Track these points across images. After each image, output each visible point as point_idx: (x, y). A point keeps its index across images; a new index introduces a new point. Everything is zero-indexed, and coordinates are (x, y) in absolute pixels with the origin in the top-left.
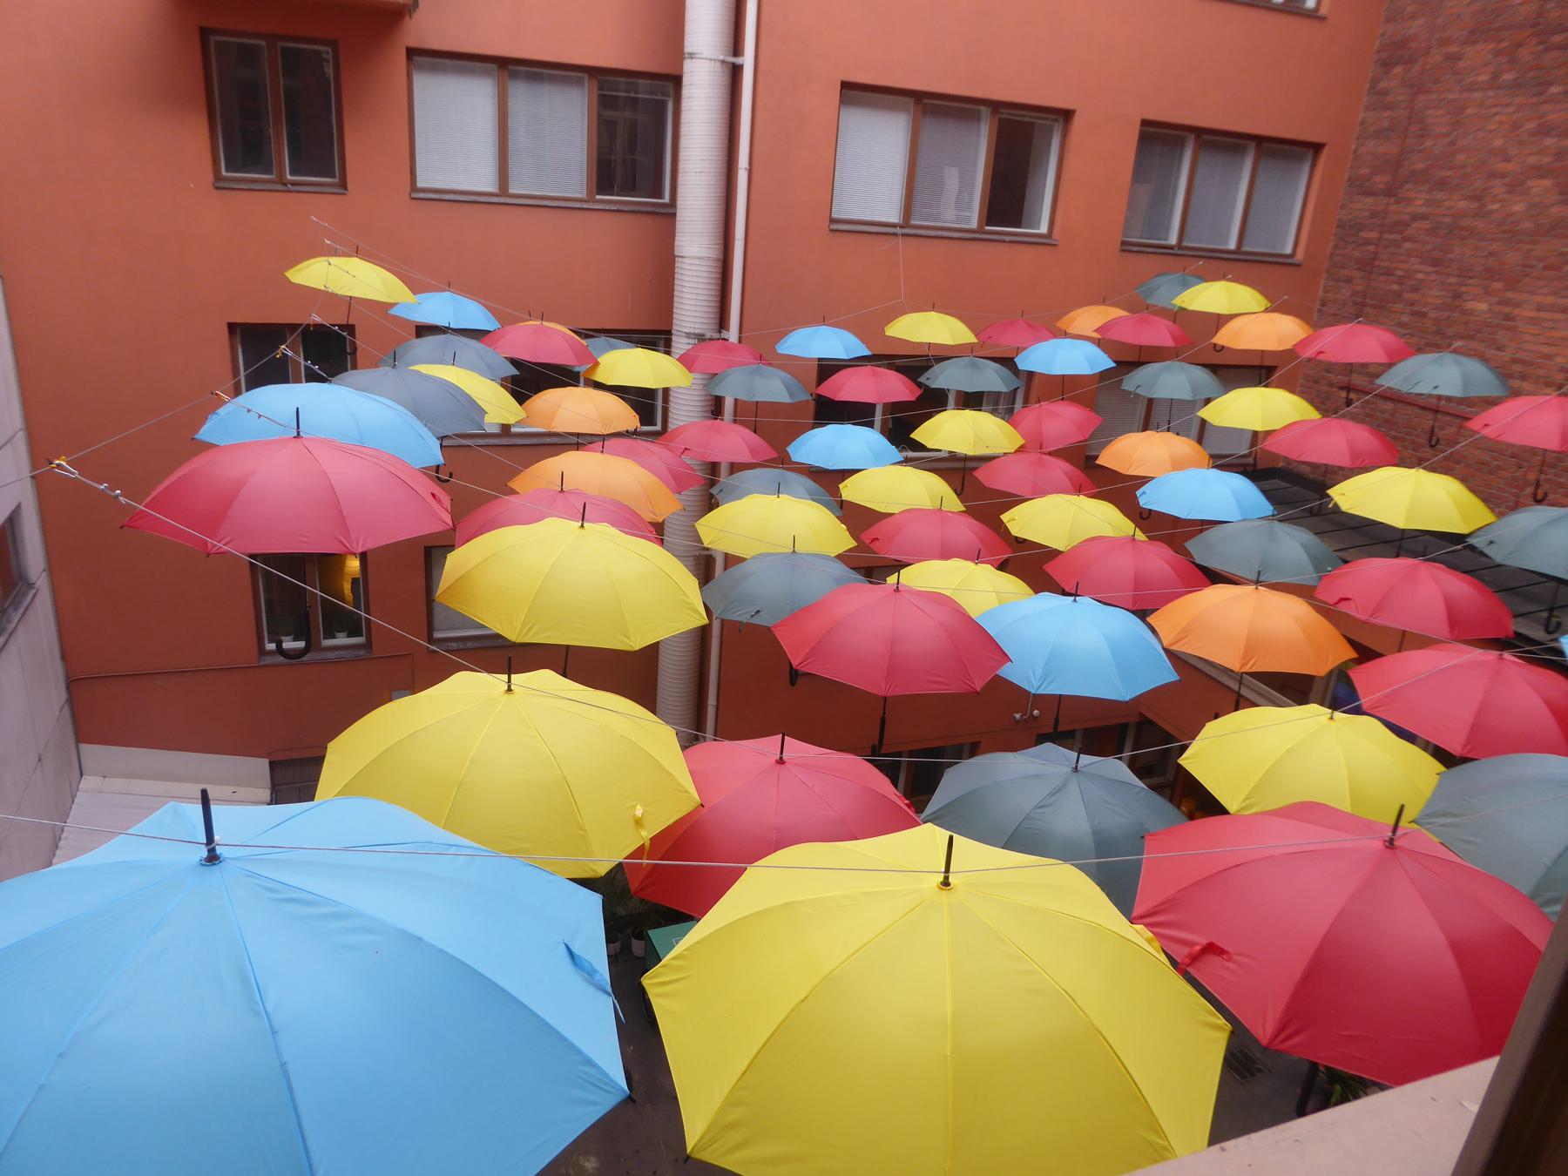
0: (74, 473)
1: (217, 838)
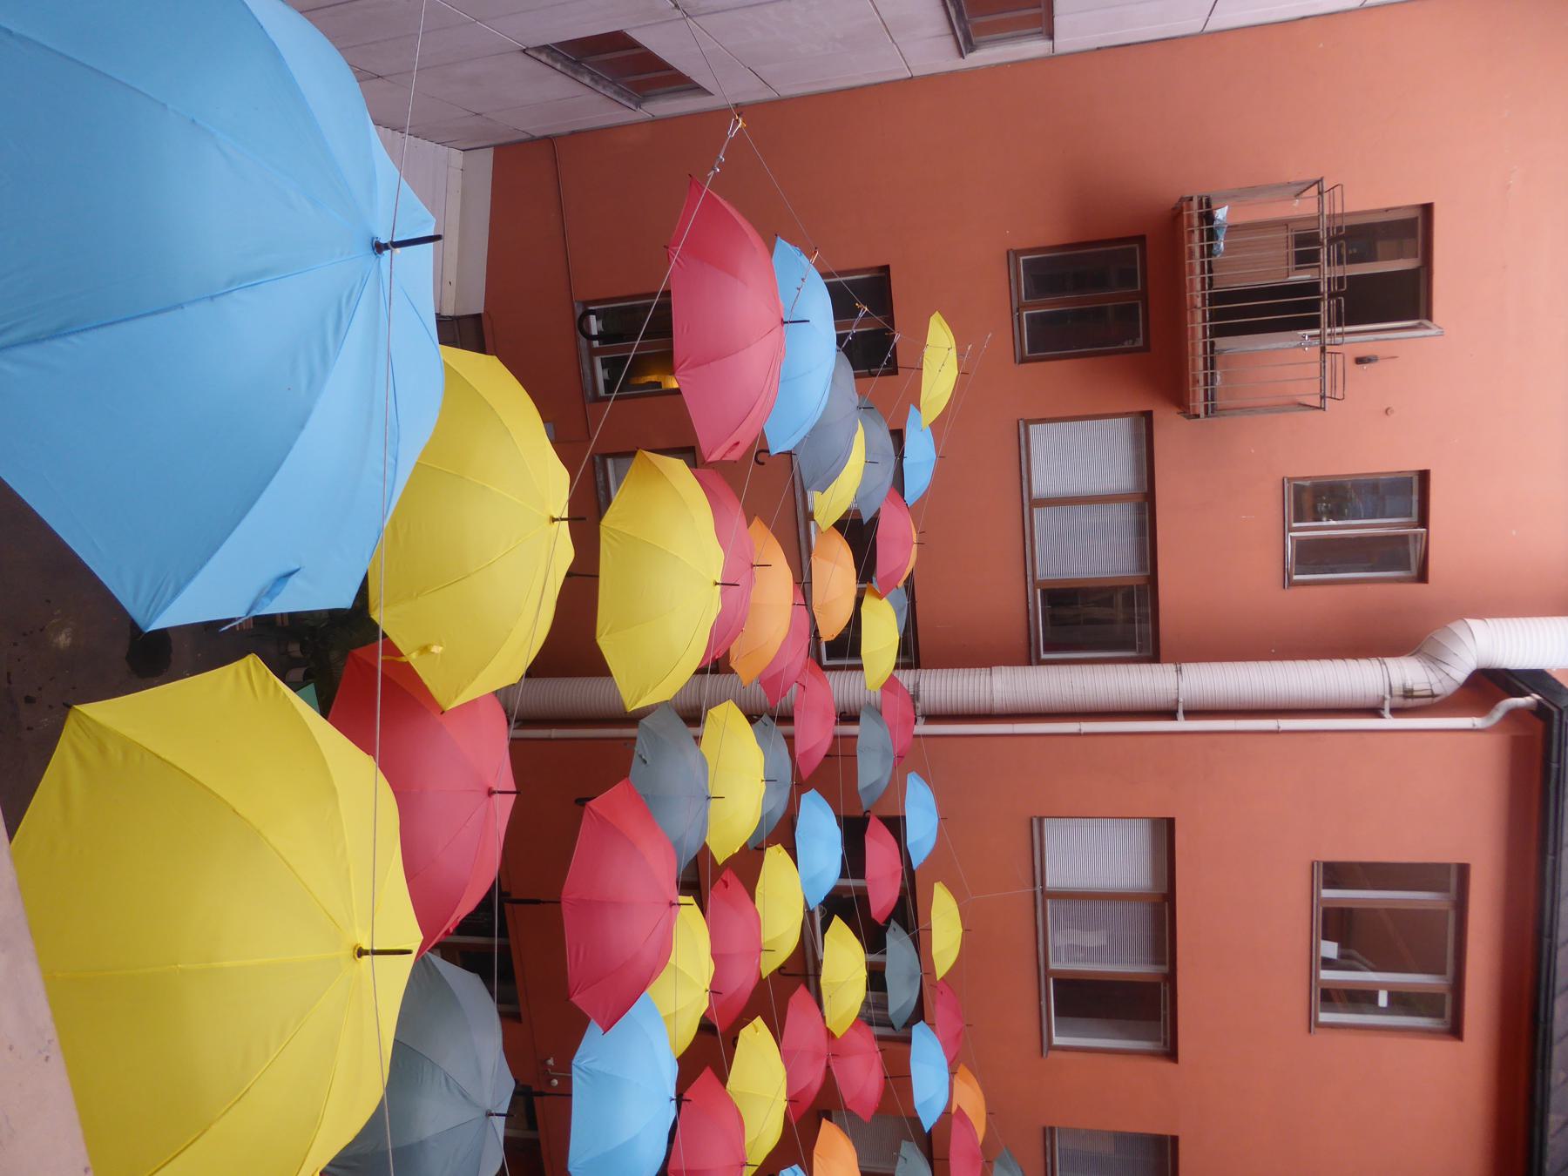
0: (732, 133)
1: (398, 250)
